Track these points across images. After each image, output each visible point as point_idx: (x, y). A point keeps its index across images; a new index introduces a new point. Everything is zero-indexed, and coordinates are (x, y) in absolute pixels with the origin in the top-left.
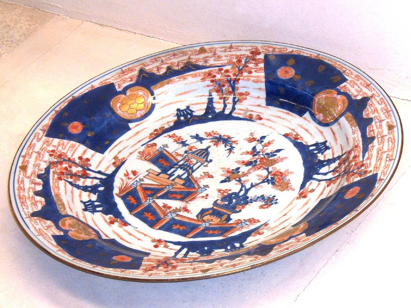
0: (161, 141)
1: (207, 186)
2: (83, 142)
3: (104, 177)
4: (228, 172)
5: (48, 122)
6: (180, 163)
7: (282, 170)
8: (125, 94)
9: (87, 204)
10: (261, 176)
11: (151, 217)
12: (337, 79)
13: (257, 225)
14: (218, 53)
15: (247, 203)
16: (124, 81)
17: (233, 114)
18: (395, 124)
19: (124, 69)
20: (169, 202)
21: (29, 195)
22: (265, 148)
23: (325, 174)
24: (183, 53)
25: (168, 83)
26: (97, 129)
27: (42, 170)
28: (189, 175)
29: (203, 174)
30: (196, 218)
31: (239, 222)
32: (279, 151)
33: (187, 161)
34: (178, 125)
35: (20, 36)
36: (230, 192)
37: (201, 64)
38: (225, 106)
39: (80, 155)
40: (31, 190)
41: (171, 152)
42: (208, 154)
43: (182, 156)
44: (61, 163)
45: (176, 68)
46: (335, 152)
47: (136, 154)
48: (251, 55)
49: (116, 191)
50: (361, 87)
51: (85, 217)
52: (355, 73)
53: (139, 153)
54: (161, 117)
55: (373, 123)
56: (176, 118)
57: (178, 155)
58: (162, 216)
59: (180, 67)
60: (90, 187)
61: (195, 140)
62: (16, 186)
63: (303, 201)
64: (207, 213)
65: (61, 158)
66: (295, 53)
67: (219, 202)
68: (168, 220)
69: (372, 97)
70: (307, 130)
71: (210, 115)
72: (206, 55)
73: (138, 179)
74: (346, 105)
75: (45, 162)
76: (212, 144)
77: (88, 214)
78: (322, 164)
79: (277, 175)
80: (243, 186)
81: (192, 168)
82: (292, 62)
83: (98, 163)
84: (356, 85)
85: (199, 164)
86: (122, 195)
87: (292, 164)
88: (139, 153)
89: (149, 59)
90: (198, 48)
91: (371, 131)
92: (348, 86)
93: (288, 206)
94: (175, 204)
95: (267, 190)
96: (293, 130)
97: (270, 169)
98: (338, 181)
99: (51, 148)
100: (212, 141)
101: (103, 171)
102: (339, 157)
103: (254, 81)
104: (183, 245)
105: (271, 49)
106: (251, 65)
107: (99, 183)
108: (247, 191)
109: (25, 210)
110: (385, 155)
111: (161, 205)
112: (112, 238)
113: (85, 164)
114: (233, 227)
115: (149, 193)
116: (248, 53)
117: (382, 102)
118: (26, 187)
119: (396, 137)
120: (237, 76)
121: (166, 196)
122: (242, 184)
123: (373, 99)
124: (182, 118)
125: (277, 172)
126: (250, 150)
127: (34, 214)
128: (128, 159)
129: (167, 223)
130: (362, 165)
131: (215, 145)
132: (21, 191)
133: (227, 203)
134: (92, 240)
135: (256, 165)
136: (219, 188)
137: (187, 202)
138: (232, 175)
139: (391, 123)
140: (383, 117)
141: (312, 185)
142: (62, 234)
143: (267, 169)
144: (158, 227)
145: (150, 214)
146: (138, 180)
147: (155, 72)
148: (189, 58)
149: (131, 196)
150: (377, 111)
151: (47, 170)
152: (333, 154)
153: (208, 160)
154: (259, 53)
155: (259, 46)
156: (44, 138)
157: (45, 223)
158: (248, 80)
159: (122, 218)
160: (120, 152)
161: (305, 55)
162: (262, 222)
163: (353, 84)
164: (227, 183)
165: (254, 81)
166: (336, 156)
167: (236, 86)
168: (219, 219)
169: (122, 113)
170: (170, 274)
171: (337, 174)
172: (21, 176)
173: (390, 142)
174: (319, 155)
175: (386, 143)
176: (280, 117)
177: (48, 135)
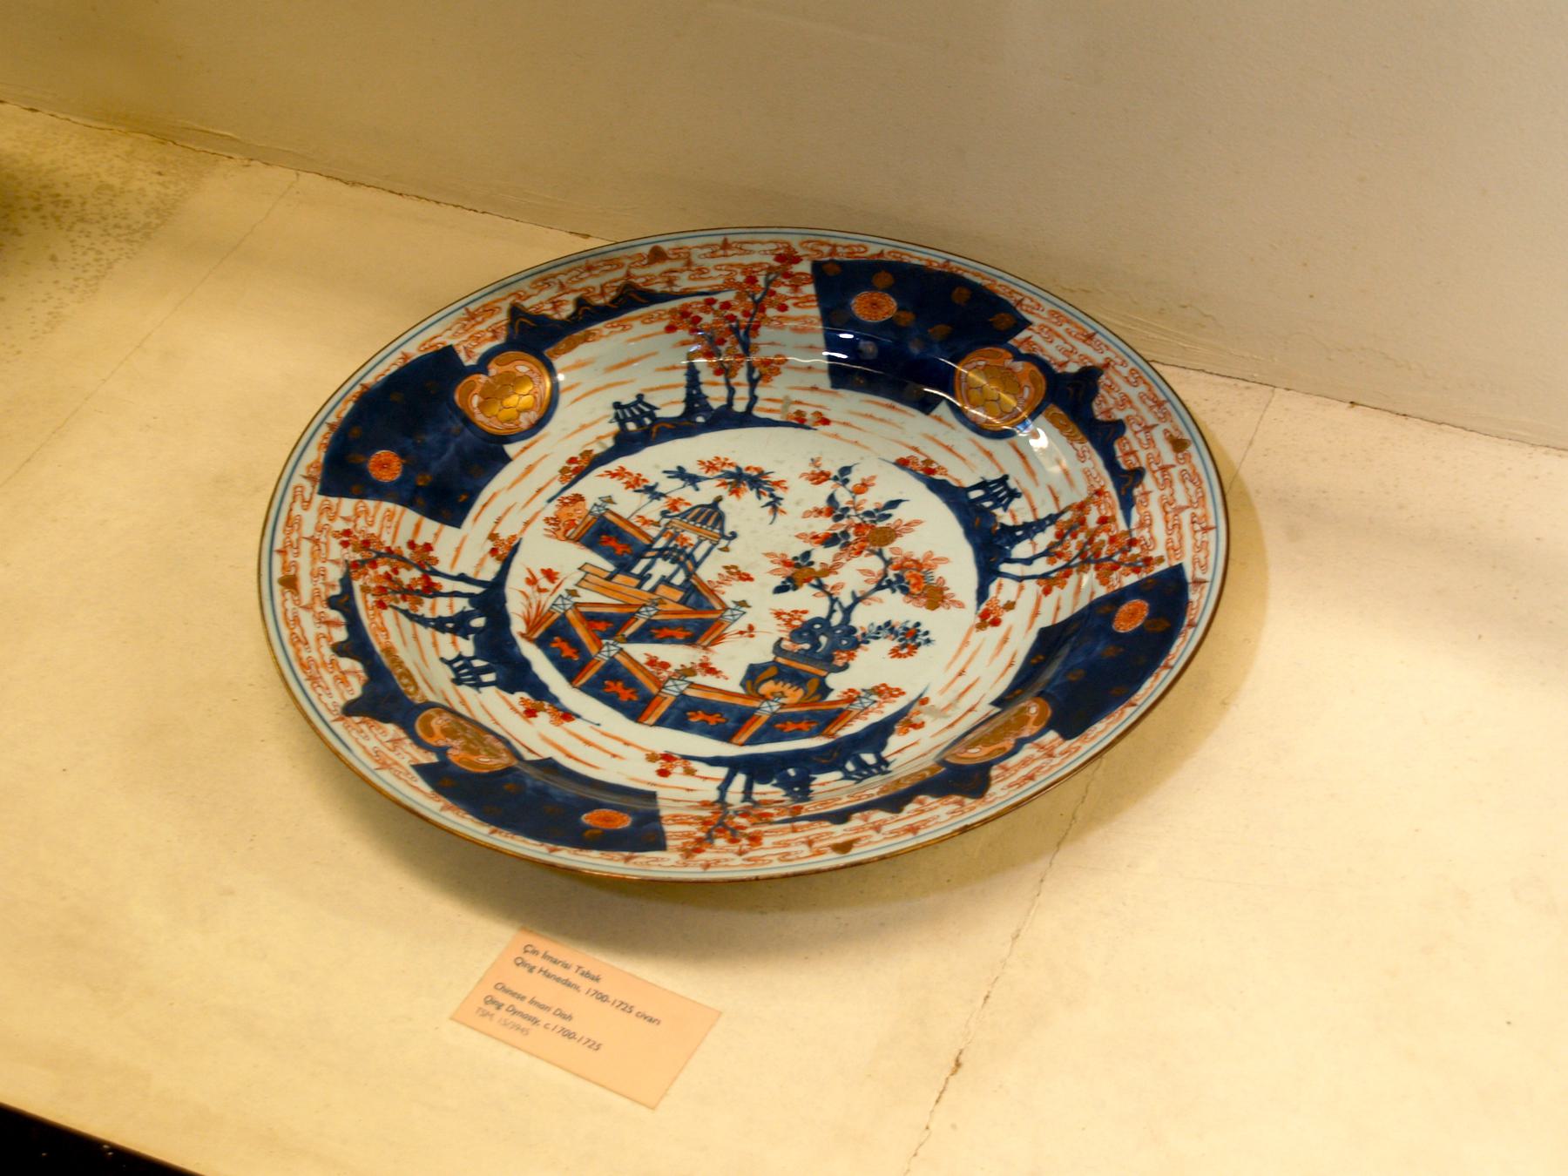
0: (594, 487)
1: (743, 604)
2: (408, 503)
3: (477, 590)
4: (786, 564)
5: (315, 455)
6: (660, 544)
7: (918, 555)
8: (486, 372)
9: (456, 665)
10: (870, 573)
11: (629, 695)
12: (1002, 321)
13: (900, 703)
14: (698, 262)
15: (856, 645)
16: (478, 340)
17: (756, 413)
18: (1186, 436)
19: (472, 307)
20: (663, 652)
21: (322, 656)
22: (859, 498)
23: (1028, 562)
24: (610, 262)
25: (585, 340)
26: (435, 466)
27: (333, 586)
28: (690, 574)
29: (724, 572)
30: (740, 690)
31: (851, 697)
32: (894, 504)
33: (674, 537)
34: (625, 444)
35: (147, 214)
36: (806, 617)
37: (658, 288)
38: (732, 391)
39: (409, 537)
40: (323, 641)
41: (626, 516)
42: (721, 518)
43: (657, 524)
44: (374, 564)
45: (601, 301)
46: (1037, 503)
47: (539, 526)
48: (777, 264)
49: (518, 627)
50: (1070, 340)
51: (463, 702)
52: (1048, 307)
53: (547, 520)
54: (576, 427)
55: (1128, 434)
56: (615, 427)
57: (646, 522)
58: (655, 690)
59: (608, 299)
60: (450, 619)
61: (678, 483)
62: (285, 633)
63: (993, 634)
64: (766, 674)
65: (370, 552)
66: (890, 258)
67: (786, 644)
68: (670, 700)
69: (1107, 365)
70: (950, 449)
71: (699, 417)
72: (667, 265)
73: (561, 591)
74: (1042, 386)
75: (336, 562)
76: (723, 491)
77: (466, 691)
78: (1012, 535)
79: (909, 568)
80: (833, 601)
81: (690, 556)
82: (885, 279)
83: (453, 553)
84: (1059, 336)
85: (706, 545)
86: (536, 635)
87: (936, 535)
88: (547, 520)
89: (528, 281)
90: (646, 250)
91: (1127, 454)
92: (1037, 339)
93: (960, 650)
94: (677, 655)
95: (894, 607)
96: (916, 449)
97: (887, 554)
98: (1072, 580)
99: (340, 525)
100: (724, 484)
101: (470, 573)
102: (1052, 519)
103: (795, 330)
104: (734, 765)
105: (826, 249)
106: (783, 290)
107: (469, 608)
108: (848, 612)
109: (325, 698)
110: (1185, 517)
111: (643, 660)
112: (546, 755)
113: (423, 557)
114: (841, 711)
115: (602, 627)
116: (770, 260)
117: (1136, 378)
118: (311, 637)
119: (1200, 470)
120: (752, 316)
121: (647, 634)
122: (830, 595)
123: (1110, 372)
124: (631, 426)
125: (906, 559)
126: (822, 504)
127: (350, 709)
128: (521, 532)
129: (672, 707)
130: (1133, 543)
131: (732, 492)
132: (300, 646)
133: (807, 646)
134: (509, 770)
135: (847, 544)
136: (778, 608)
137: (705, 648)
138: (797, 573)
139: (1176, 434)
140: (1151, 420)
141: (1002, 591)
142: (434, 759)
143: (880, 554)
144: (652, 720)
145: (620, 684)
146: (565, 594)
147: (549, 313)
148: (628, 275)
149: (553, 633)
150: (1130, 402)
151: (346, 583)
152: (1034, 510)
153: (727, 531)
154: (797, 260)
155: (795, 241)
156: (318, 499)
157: (384, 732)
158: (781, 327)
159: (554, 700)
160: (498, 521)
161: (915, 262)
162: (912, 695)
163: (1051, 335)
164: (790, 594)
165: (795, 330)
166: (1042, 514)
167: (753, 341)
168: (801, 692)
169: (486, 421)
170: (755, 859)
171: (1060, 563)
172: (290, 605)
173: (1189, 485)
174: (999, 512)
175: (1178, 487)
176: (871, 416)
177: (325, 491)
